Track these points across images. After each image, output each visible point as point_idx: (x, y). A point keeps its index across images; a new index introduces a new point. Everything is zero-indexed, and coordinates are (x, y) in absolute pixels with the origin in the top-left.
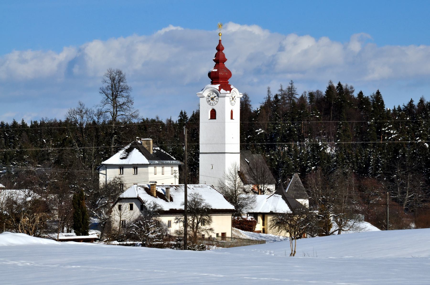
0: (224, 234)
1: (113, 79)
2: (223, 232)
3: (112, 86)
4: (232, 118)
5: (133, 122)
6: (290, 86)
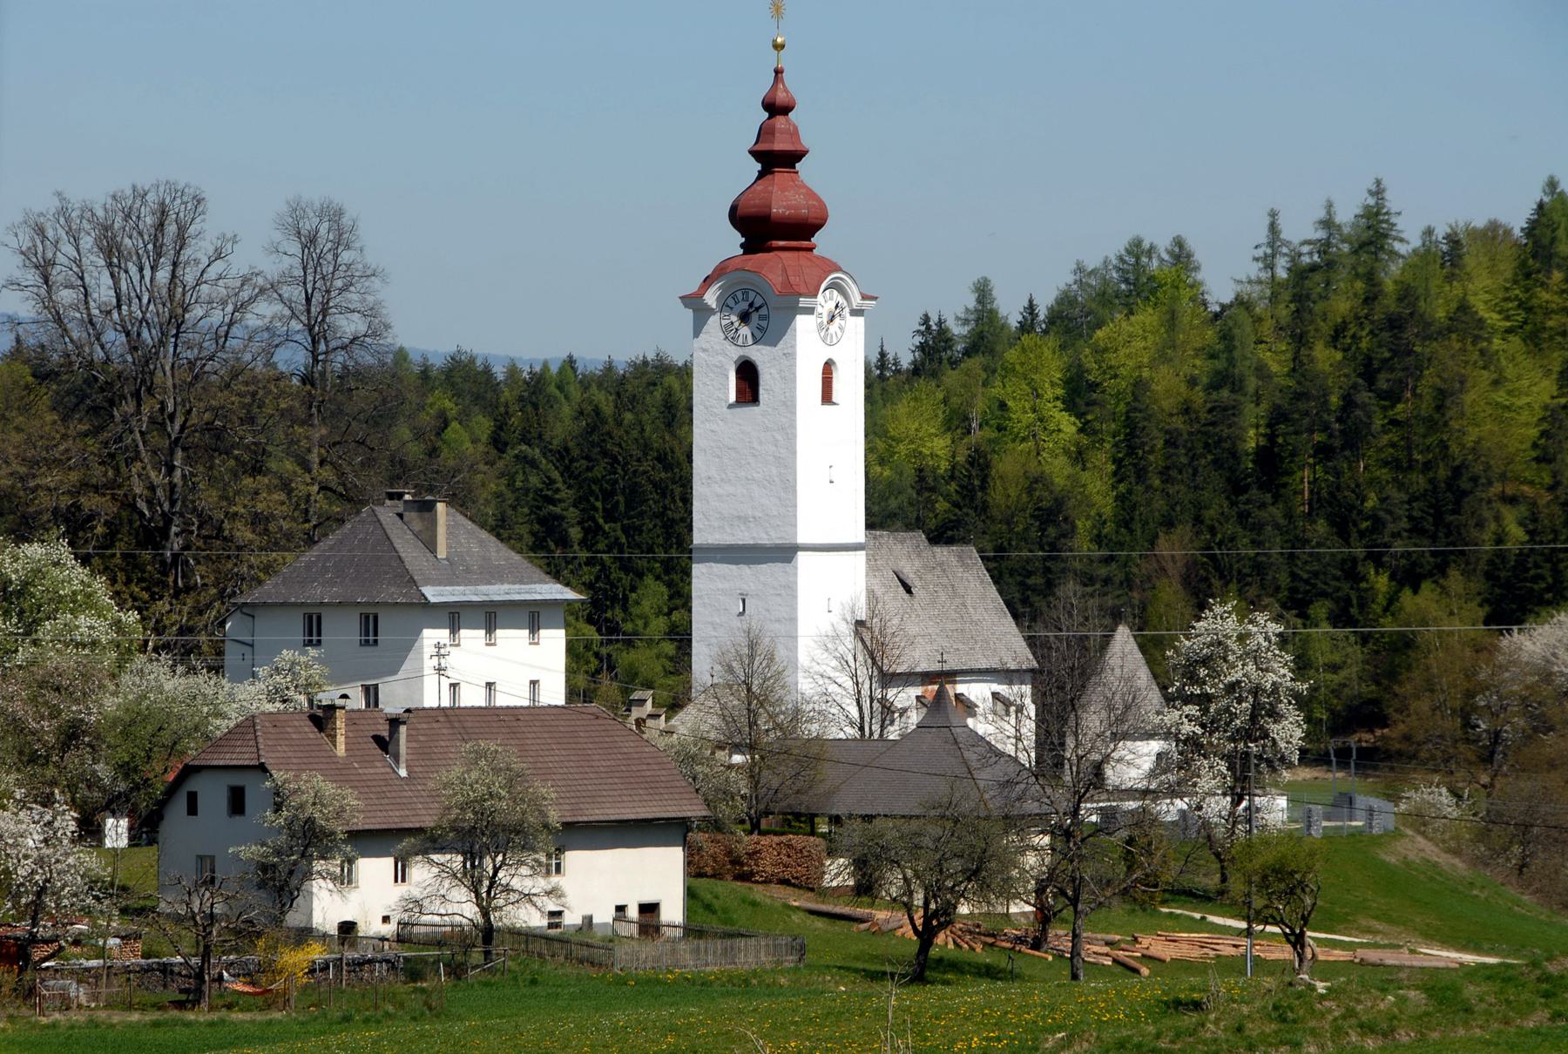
0: (649, 909)
1: (310, 241)
2: (649, 898)
3: (305, 269)
4: (827, 397)
5: (1422, 310)
6: (1371, 201)
